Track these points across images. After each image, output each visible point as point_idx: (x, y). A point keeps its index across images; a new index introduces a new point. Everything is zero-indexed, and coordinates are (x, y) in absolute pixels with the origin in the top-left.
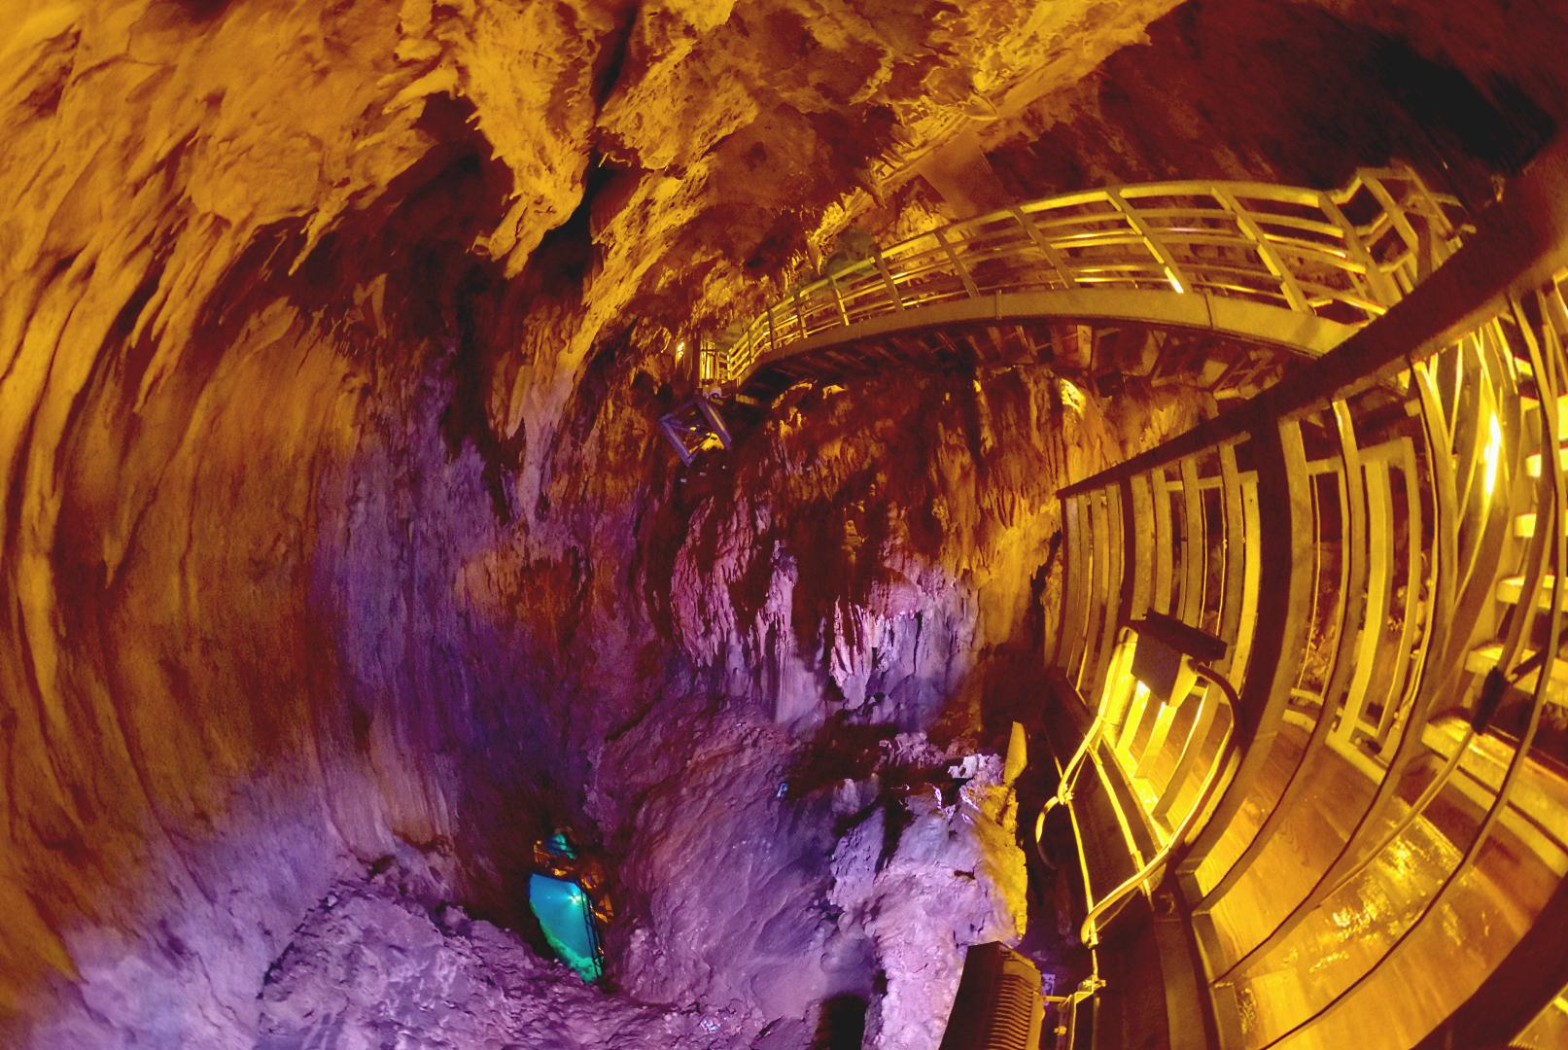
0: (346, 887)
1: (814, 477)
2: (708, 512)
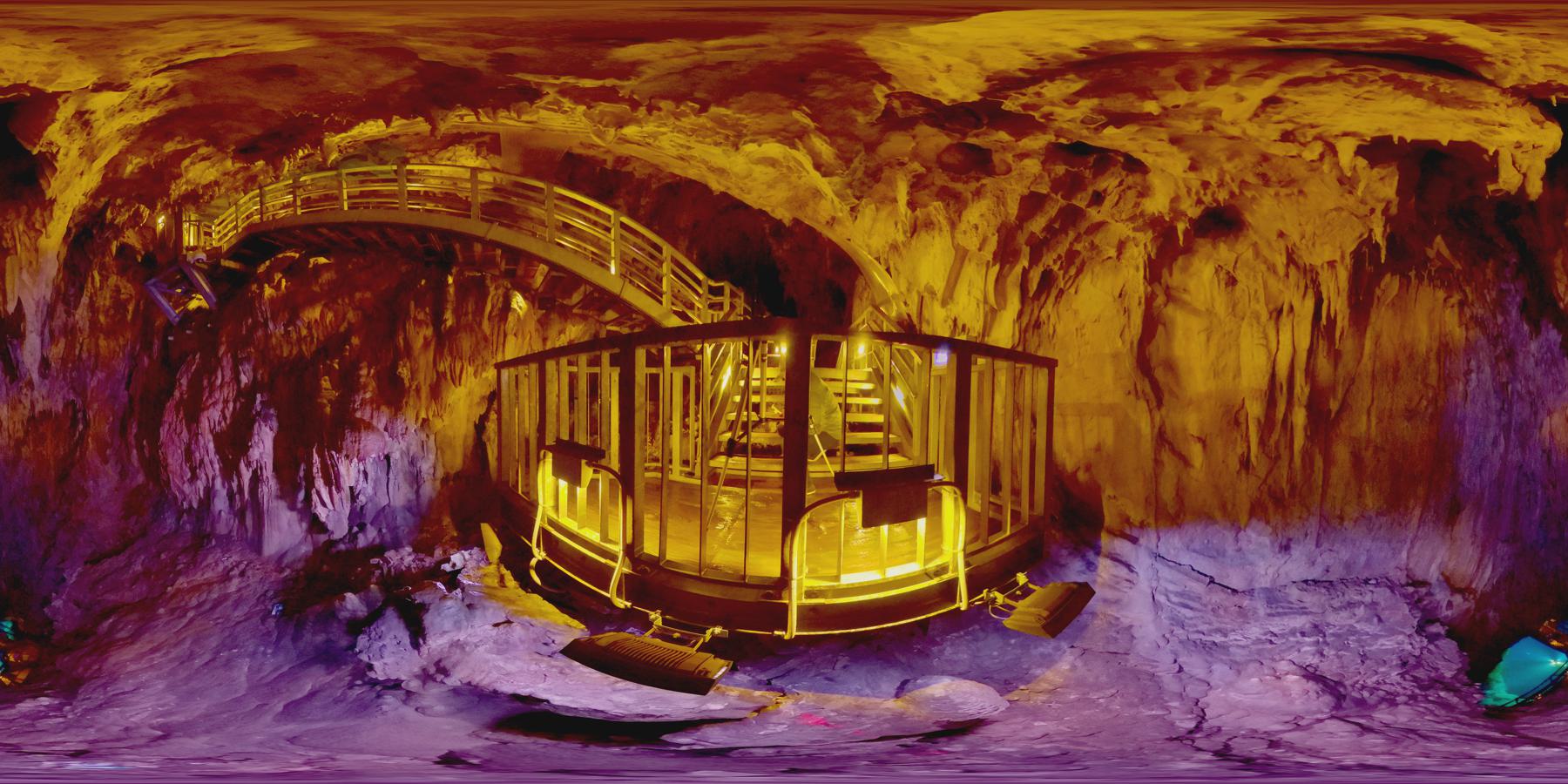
1: (294, 336)
2: (194, 367)
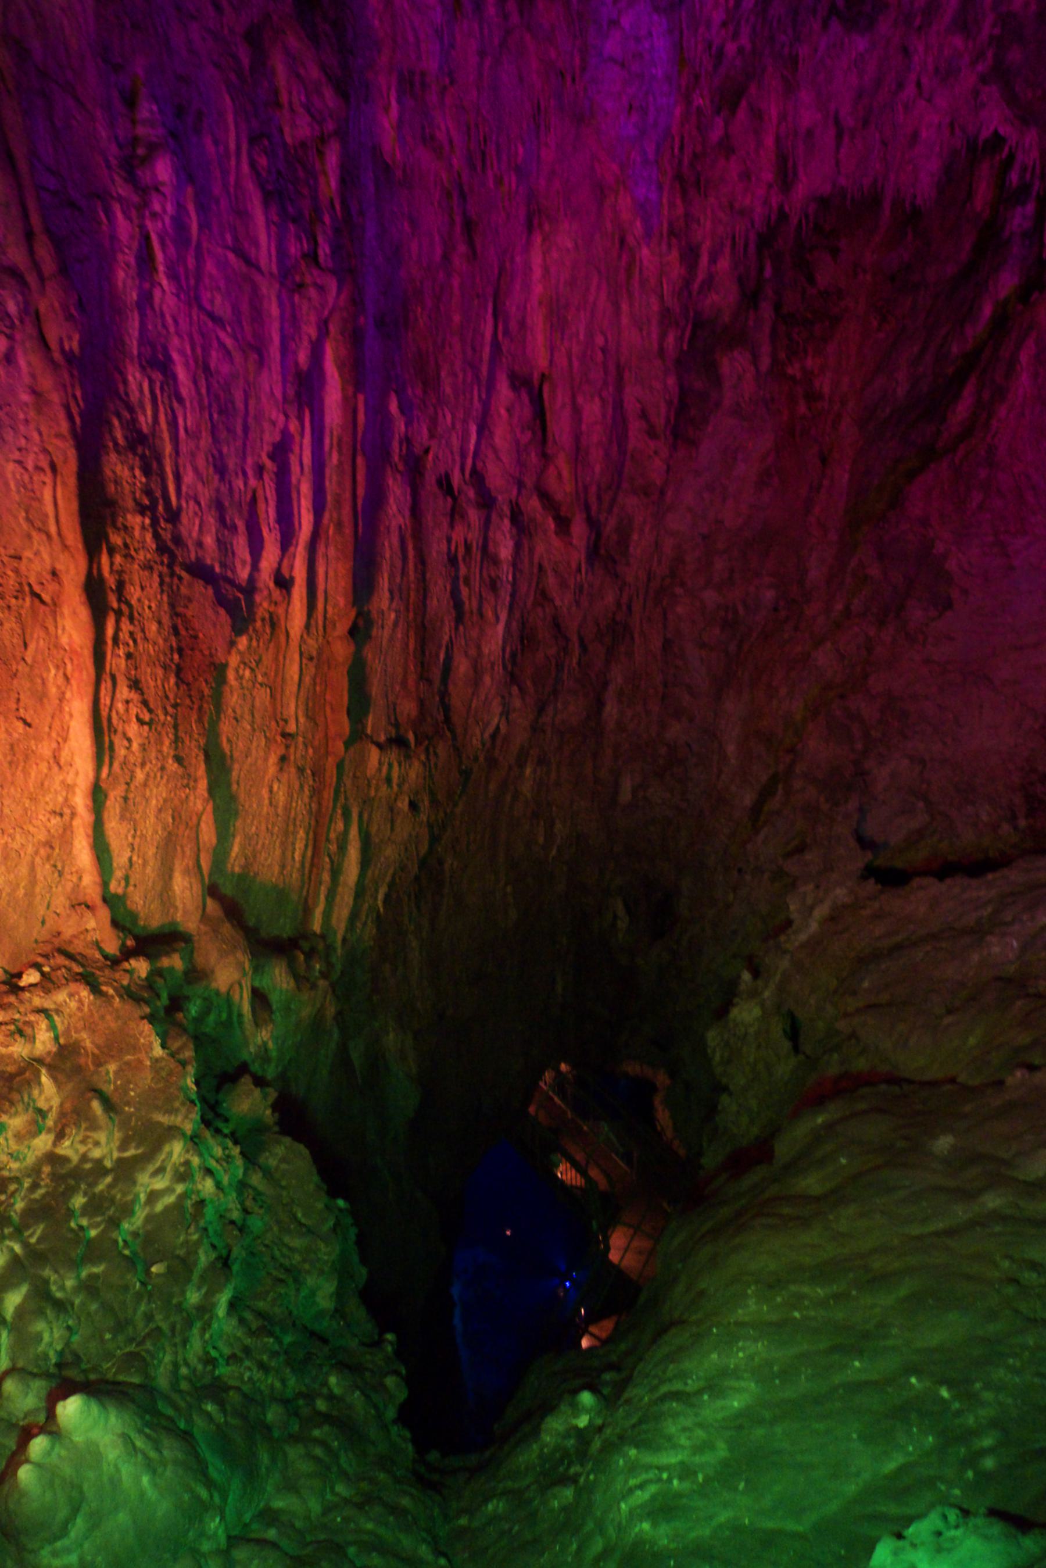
0: (67, 962)
